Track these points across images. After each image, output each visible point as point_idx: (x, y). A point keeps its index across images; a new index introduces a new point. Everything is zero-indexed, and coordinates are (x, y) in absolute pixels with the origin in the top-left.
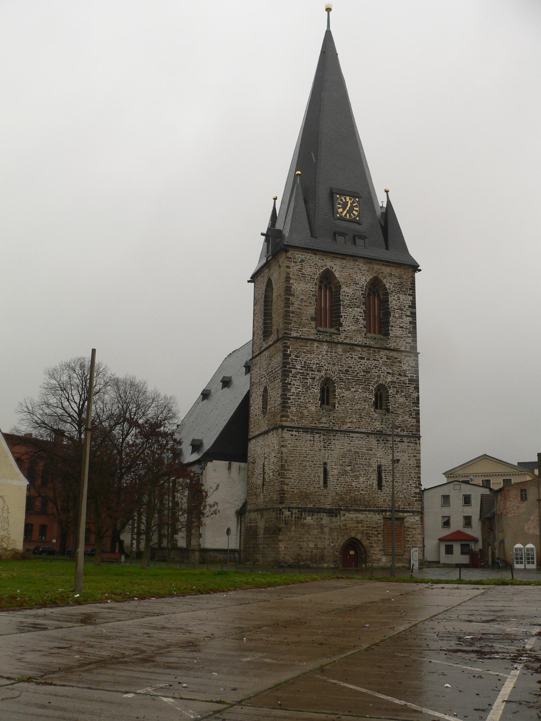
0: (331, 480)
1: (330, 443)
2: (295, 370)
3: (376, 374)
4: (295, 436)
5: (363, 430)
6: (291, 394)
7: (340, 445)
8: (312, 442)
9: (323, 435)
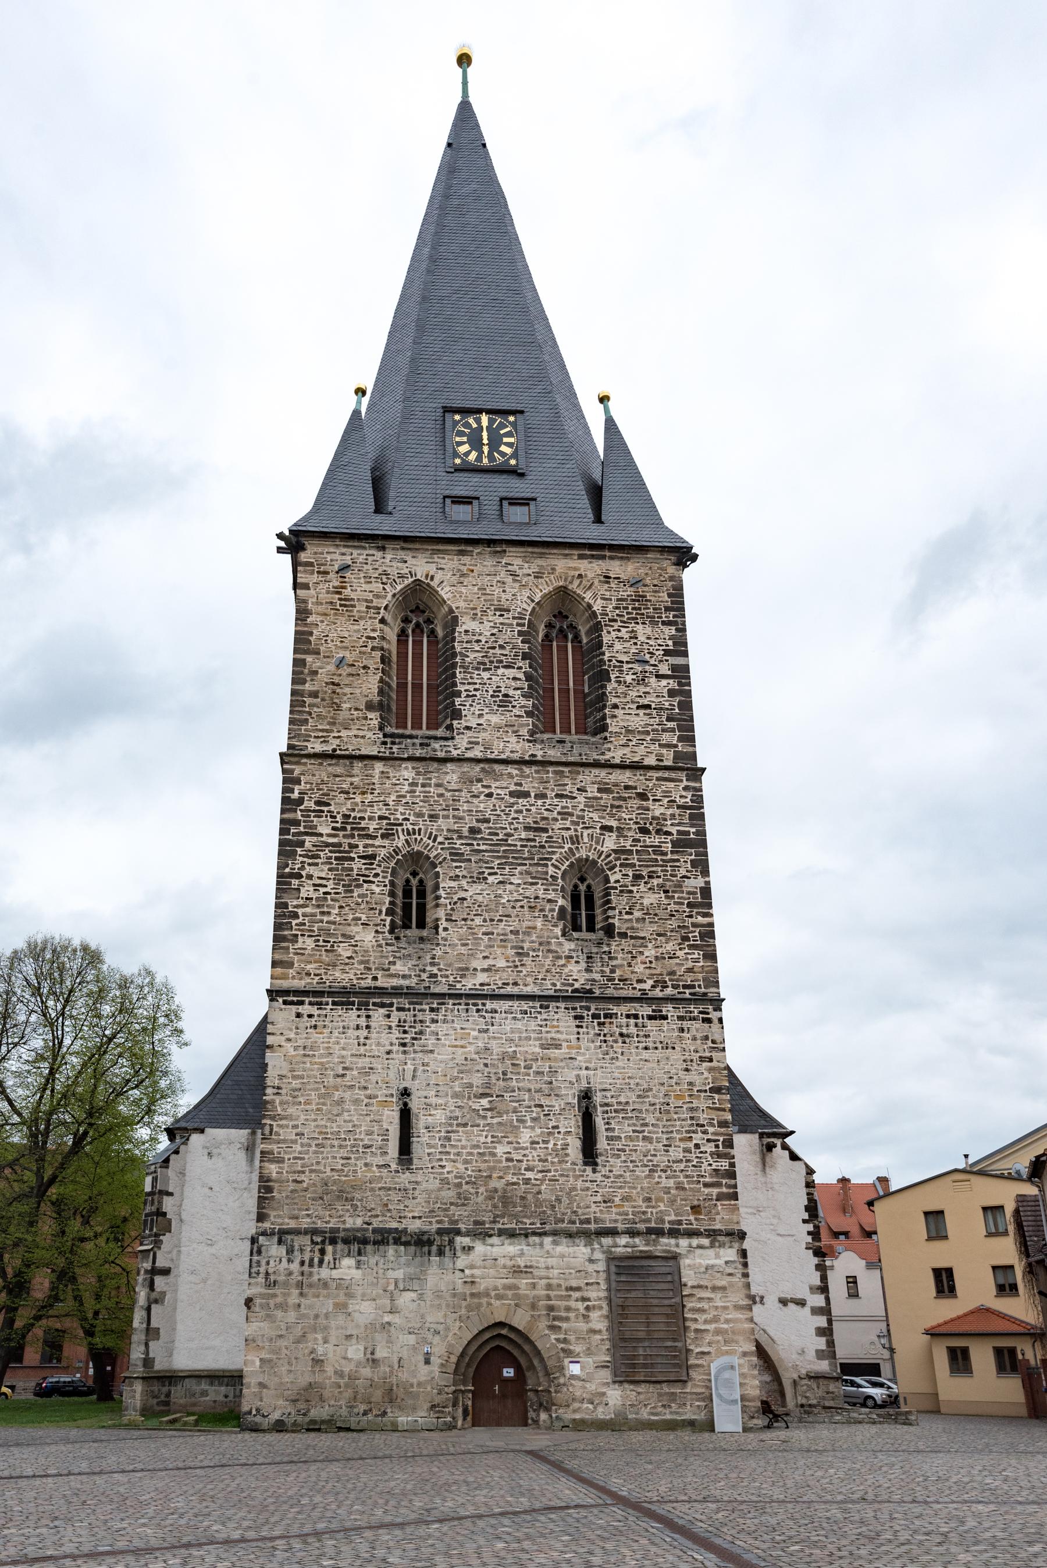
0: (425, 1139)
1: (421, 1033)
4: (310, 1016)
6: (301, 902)
9: (399, 1009)
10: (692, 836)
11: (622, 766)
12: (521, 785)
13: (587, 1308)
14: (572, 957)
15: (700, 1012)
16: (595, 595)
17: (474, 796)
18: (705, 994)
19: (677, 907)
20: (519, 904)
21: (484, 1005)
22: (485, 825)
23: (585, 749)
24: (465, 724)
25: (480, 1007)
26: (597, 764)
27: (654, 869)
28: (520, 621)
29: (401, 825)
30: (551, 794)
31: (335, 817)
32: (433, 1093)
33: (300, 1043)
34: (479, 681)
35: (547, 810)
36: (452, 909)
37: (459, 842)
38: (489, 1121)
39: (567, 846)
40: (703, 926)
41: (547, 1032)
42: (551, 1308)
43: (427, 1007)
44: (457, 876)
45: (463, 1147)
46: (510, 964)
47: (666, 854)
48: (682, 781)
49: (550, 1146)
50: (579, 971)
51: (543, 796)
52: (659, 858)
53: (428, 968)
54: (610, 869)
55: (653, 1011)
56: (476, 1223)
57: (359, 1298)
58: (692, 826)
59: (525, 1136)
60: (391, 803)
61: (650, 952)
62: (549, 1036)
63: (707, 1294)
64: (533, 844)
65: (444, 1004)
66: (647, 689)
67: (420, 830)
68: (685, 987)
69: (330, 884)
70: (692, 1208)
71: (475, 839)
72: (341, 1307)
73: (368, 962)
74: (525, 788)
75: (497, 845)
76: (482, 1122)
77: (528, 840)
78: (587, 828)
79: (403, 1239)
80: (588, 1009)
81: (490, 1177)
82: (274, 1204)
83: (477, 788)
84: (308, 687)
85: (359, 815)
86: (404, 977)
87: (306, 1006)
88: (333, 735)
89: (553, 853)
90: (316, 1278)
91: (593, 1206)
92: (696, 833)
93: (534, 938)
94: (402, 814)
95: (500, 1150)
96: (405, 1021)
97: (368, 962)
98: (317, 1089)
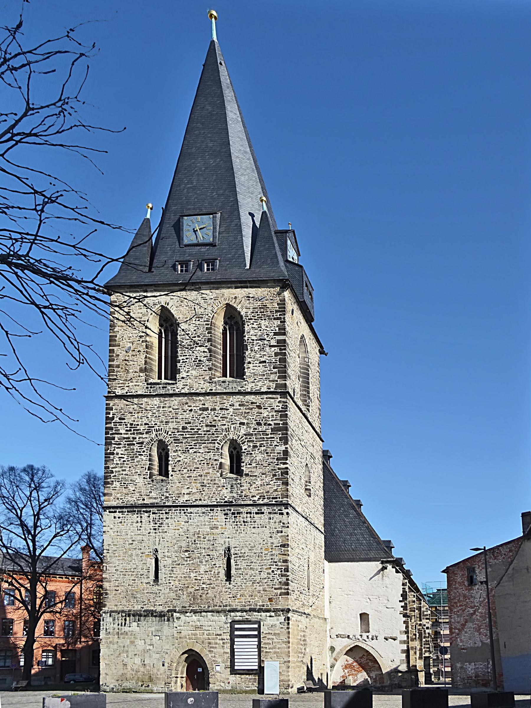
0: (163, 571)
1: (162, 524)
2: (119, 436)
3: (224, 427)
4: (119, 518)
5: (205, 503)
6: (114, 466)
7: (175, 524)
8: (140, 524)
9: (153, 513)
10: (281, 425)
11: (250, 393)
12: (204, 405)
13: (224, 643)
14: (224, 486)
15: (279, 510)
16: (242, 307)
17: (185, 411)
18: (282, 501)
19: (272, 460)
20: (202, 462)
21: (187, 510)
22: (189, 425)
23: (235, 385)
24: (181, 376)
25: (185, 511)
26: (239, 393)
27: (261, 443)
28: (207, 323)
29: (154, 427)
30: (218, 408)
31: (127, 425)
32: (167, 551)
33: (116, 530)
34: (188, 354)
35: (216, 416)
36: (175, 466)
37: (177, 434)
38: (188, 562)
39: (224, 433)
40: (283, 469)
41: (213, 522)
42: (210, 643)
43: (164, 512)
44: (177, 450)
45: (178, 574)
46: (199, 491)
47: (268, 435)
48: (278, 398)
49: (212, 573)
50: (227, 493)
51: (215, 409)
52: (265, 437)
53: (165, 494)
54: (243, 444)
55: (258, 510)
56: (183, 607)
57: (139, 639)
58: (281, 421)
59: (202, 569)
60: (150, 417)
61: (259, 482)
62: (213, 523)
63: (270, 637)
64: (209, 433)
65: (171, 510)
66: (265, 353)
67: (161, 429)
68: (273, 498)
69: (126, 457)
70: (269, 599)
71: (184, 432)
72: (132, 642)
73: (140, 492)
74: (206, 406)
75: (193, 434)
76: (185, 563)
77: (207, 431)
78: (233, 424)
79: (154, 614)
80: (230, 510)
81: (188, 587)
82: (108, 600)
83: (186, 407)
84: (115, 363)
85: (136, 423)
86: (155, 498)
87: (117, 513)
88: (126, 385)
89: (218, 437)
90: (123, 631)
91: (229, 599)
92: (283, 424)
93: (209, 478)
94: (154, 422)
95: (192, 575)
96: (156, 519)
97: (140, 492)
98: (122, 550)
